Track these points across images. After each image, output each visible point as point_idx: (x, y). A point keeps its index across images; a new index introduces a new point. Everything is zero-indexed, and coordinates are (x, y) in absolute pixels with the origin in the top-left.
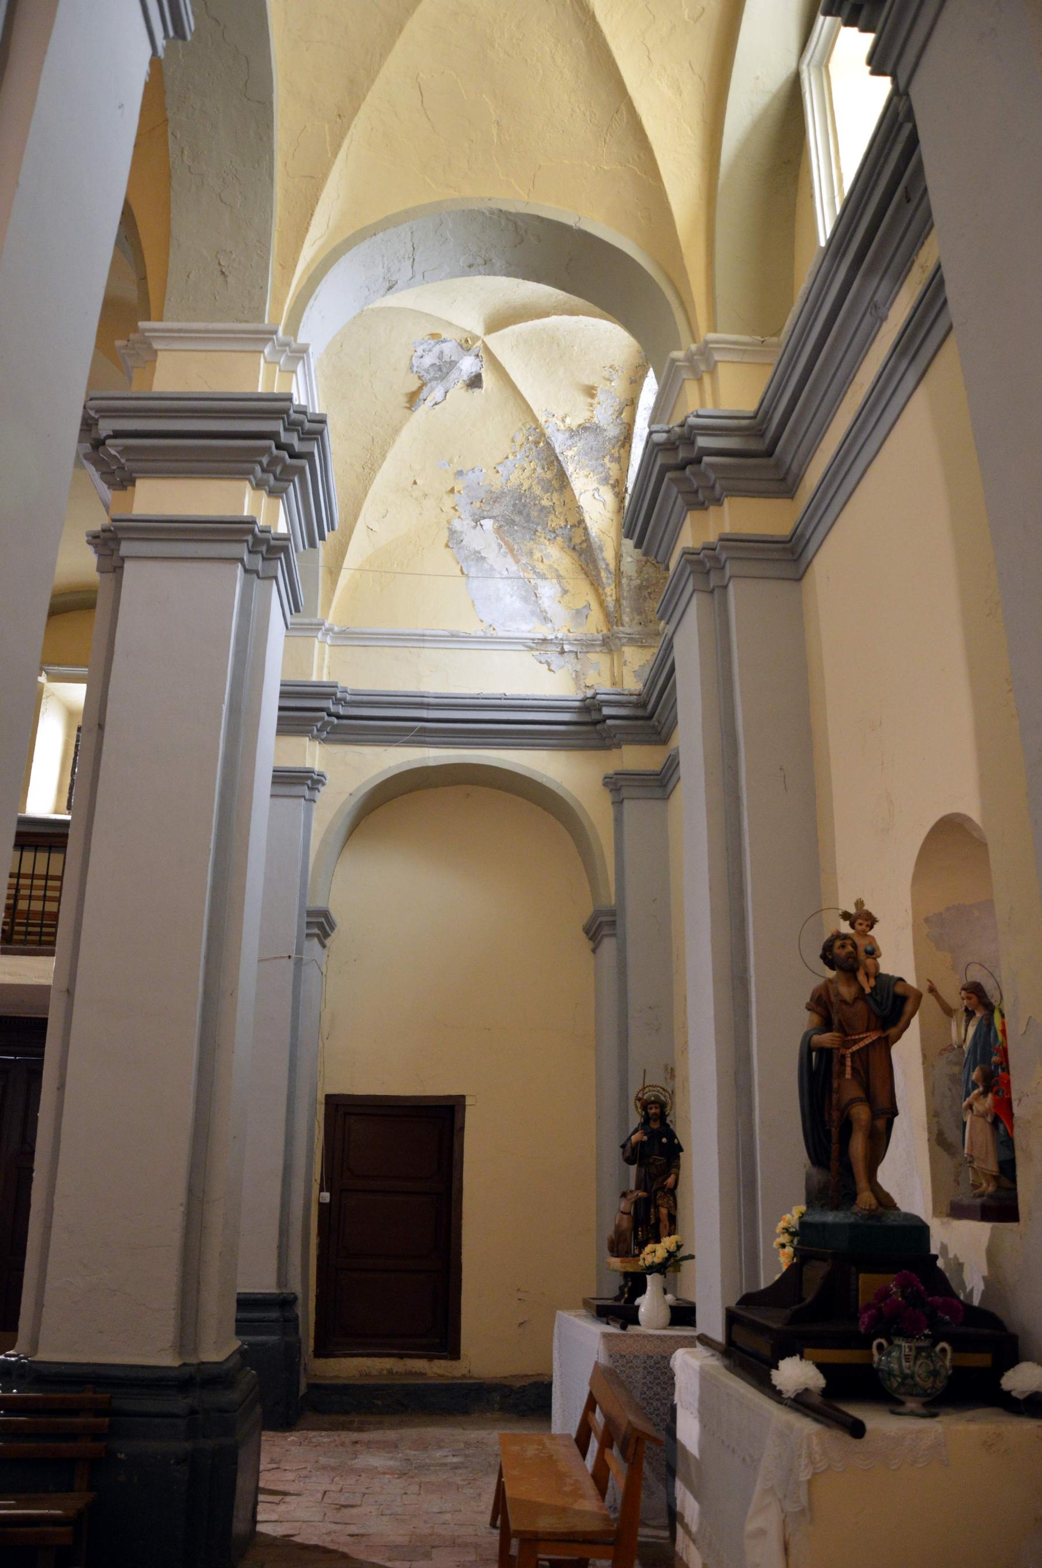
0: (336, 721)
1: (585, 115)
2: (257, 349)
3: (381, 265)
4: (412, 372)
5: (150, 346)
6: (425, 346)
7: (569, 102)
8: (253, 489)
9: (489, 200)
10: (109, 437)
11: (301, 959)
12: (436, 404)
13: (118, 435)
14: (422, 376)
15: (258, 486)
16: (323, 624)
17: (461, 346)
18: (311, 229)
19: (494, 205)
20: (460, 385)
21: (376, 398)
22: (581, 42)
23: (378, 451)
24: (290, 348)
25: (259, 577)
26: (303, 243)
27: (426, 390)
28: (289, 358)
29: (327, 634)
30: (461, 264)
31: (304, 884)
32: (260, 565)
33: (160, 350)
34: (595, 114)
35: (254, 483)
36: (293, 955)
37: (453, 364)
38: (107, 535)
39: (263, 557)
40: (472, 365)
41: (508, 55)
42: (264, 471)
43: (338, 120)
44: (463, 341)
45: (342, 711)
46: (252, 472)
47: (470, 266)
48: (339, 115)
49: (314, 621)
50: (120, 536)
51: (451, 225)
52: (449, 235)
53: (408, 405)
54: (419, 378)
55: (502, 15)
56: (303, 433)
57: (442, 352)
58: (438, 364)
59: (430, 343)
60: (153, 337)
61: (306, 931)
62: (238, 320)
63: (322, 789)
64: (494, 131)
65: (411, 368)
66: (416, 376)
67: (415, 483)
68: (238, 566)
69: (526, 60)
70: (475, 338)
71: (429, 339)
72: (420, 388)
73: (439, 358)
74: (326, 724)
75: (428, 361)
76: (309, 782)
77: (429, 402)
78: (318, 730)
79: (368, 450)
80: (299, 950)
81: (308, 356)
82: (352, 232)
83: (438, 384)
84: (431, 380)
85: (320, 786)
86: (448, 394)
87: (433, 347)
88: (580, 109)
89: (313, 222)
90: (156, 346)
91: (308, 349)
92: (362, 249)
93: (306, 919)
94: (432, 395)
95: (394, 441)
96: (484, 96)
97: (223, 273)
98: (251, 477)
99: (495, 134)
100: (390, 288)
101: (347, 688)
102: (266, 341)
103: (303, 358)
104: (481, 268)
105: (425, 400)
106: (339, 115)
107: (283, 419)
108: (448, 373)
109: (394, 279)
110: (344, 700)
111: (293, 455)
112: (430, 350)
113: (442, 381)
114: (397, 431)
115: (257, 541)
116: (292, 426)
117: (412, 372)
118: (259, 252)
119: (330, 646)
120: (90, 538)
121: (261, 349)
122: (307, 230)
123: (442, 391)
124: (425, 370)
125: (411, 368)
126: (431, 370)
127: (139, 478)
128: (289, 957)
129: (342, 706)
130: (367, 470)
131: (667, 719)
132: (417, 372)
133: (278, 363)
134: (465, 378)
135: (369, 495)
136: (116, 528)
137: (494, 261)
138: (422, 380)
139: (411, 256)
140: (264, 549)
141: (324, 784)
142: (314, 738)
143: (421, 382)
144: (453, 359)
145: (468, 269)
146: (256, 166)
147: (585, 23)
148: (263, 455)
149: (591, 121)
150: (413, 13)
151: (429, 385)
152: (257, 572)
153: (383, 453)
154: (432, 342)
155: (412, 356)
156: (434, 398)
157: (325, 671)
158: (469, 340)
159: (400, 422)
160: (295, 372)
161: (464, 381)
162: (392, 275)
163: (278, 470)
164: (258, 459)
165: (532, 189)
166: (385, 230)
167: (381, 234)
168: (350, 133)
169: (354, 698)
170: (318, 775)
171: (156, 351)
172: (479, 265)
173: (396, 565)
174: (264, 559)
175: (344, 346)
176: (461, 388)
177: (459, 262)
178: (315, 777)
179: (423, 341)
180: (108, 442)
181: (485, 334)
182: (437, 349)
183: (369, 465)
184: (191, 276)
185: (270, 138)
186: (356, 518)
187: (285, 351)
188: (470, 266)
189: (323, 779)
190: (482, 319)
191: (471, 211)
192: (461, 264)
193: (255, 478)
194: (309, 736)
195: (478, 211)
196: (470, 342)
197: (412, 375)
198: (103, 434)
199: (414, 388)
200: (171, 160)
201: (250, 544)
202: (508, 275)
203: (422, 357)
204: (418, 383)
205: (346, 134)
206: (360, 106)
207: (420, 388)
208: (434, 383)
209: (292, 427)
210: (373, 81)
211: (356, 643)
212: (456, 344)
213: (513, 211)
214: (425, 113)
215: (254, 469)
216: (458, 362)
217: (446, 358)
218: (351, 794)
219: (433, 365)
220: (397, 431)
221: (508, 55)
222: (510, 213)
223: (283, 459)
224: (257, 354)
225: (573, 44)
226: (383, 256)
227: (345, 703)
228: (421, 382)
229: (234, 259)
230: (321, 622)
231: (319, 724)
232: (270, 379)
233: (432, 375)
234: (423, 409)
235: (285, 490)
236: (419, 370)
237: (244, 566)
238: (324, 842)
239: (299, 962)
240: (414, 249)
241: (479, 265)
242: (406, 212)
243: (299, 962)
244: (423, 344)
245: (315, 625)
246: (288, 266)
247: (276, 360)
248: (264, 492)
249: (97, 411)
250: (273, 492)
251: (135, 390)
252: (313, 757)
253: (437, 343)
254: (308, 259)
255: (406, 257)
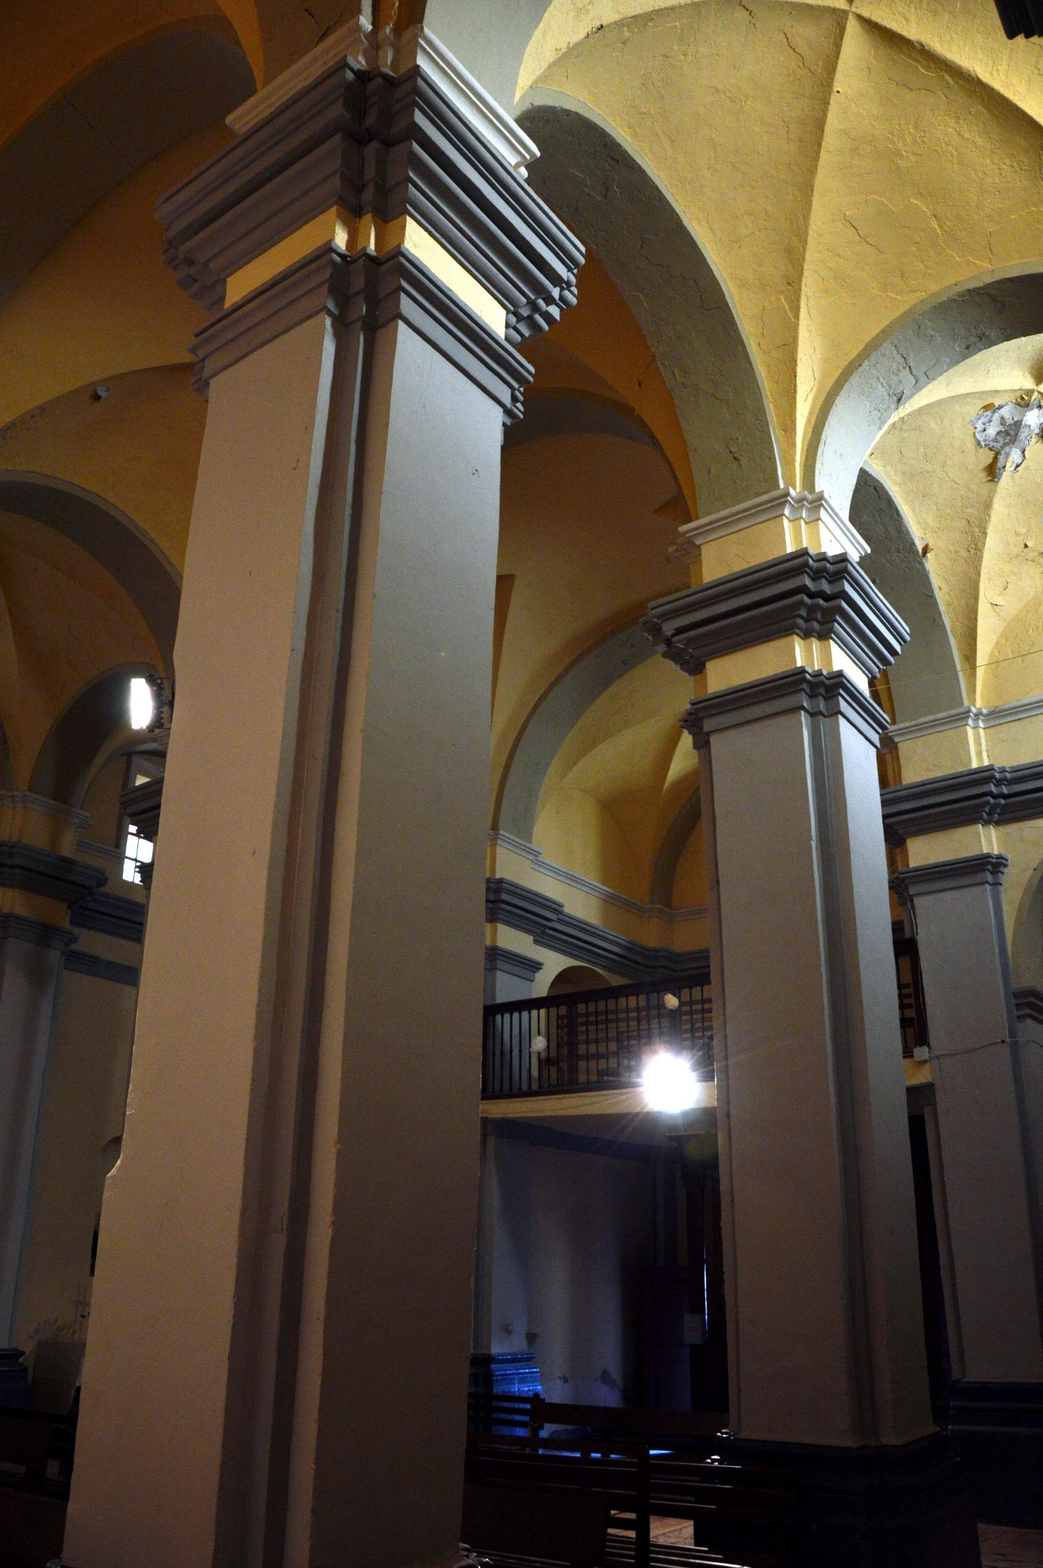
0: (1002, 801)
1: (1013, 167)
2: (778, 514)
3: (880, 386)
4: (981, 447)
5: (694, 543)
6: (983, 420)
7: (993, 163)
8: (803, 639)
9: (956, 285)
10: (674, 635)
11: (1016, 1042)
12: (1018, 466)
13: (680, 631)
14: (993, 447)
15: (806, 635)
16: (969, 711)
17: (1019, 405)
18: (799, 389)
19: (960, 289)
20: (1034, 439)
21: (957, 483)
22: (980, 107)
23: (978, 530)
24: (807, 501)
25: (825, 716)
26: (795, 403)
27: (1001, 458)
28: (809, 509)
29: (978, 719)
30: (958, 350)
31: (1005, 966)
32: (822, 705)
33: (702, 544)
34: (1021, 161)
35: (802, 634)
36: (1007, 1040)
37: (1018, 425)
38: (693, 717)
39: (824, 697)
40: (1038, 417)
41: (917, 155)
42: (806, 621)
43: (789, 287)
44: (1019, 400)
45: (1005, 790)
46: (796, 626)
47: (967, 348)
48: (789, 283)
49: (961, 710)
50: (701, 716)
51: (929, 324)
52: (932, 332)
53: (990, 478)
54: (990, 449)
55: (897, 127)
56: (830, 577)
57: (1002, 418)
58: (1003, 430)
59: (987, 415)
60: (693, 536)
61: (1016, 1013)
62: (758, 494)
63: (1006, 870)
64: (934, 224)
65: (979, 443)
66: (987, 448)
67: (1026, 546)
68: (801, 714)
69: (937, 151)
70: (1030, 392)
71: (984, 412)
72: (996, 459)
73: (1002, 424)
74: (993, 807)
75: (992, 431)
76: (990, 867)
77: (1010, 467)
78: (987, 814)
79: (966, 533)
80: (1012, 1032)
81: (826, 501)
82: (839, 372)
83: (1011, 448)
84: (1002, 448)
85: (1002, 869)
86: (1026, 453)
87: (991, 417)
88: (1005, 164)
89: (798, 382)
90: (698, 543)
91: (823, 496)
92: (855, 379)
93: (1014, 1002)
94: (1010, 460)
95: (989, 516)
96: (912, 200)
97: (735, 458)
98: (797, 631)
99: (936, 226)
100: (899, 400)
101: (1004, 767)
102: (783, 505)
103: (822, 505)
104: (979, 345)
105: (1004, 467)
106: (789, 283)
107: (806, 572)
108: (1017, 434)
109: (899, 391)
110: (1005, 779)
111: (827, 598)
112: (990, 421)
113: (1013, 443)
114: (988, 505)
115: (813, 686)
116: (817, 575)
117: (981, 447)
118: (760, 428)
119: (984, 729)
120: (682, 723)
121: (780, 513)
122: (795, 391)
123: (1019, 452)
124: (993, 441)
125: (979, 443)
126: (999, 438)
127: (708, 660)
128: (1003, 1042)
129: (1006, 785)
130: (972, 551)
131: (623, 940)
132: (985, 445)
133: (802, 518)
134: (1037, 431)
135: (982, 574)
136: (697, 710)
137: (987, 333)
138: (993, 451)
139: (905, 365)
140: (822, 691)
141: (1006, 866)
142: (986, 823)
143: (994, 452)
144: (1016, 419)
145: (966, 351)
146: (734, 359)
147: (975, 91)
148: (799, 609)
149: (1021, 169)
150: (816, 170)
151: (1003, 452)
152: (821, 713)
153: (982, 530)
154: (989, 413)
155: (974, 434)
156: (1014, 462)
157: (985, 755)
158: (1024, 396)
159: (989, 496)
160: (819, 519)
161: (1036, 434)
162: (895, 389)
163: (819, 616)
164: (796, 613)
165: (991, 257)
166: (868, 357)
167: (866, 362)
168: (803, 293)
169: (1015, 775)
170: (997, 858)
171: (699, 547)
172: (975, 343)
173: (1031, 631)
174: (825, 699)
175: (903, 452)
176: (1037, 442)
177: (955, 349)
178: (994, 861)
179: (978, 417)
180: (674, 639)
181: (1037, 385)
182: (996, 416)
183: (973, 546)
184: (712, 471)
185: (736, 331)
186: (976, 599)
187: (804, 505)
188: (967, 348)
189: (1003, 861)
190: (1027, 373)
191: (942, 304)
192: (958, 350)
193: (801, 630)
194: (980, 823)
195: (948, 300)
196: (1026, 398)
197: (981, 451)
198: (669, 633)
199: (990, 461)
200: (667, 384)
201: (808, 691)
202: (1008, 338)
203: (984, 430)
204: (992, 455)
205: (799, 296)
206: (802, 267)
207: (996, 459)
208: (1007, 449)
209: (818, 575)
210: (806, 241)
211: (1009, 719)
212: (1013, 406)
213: (981, 284)
214: (866, 241)
215: (796, 622)
216: (1022, 421)
217: (1009, 422)
218: (1035, 869)
219: (999, 433)
220: (988, 505)
221: (917, 155)
222: (979, 288)
223: (819, 606)
224: (780, 518)
225: (973, 113)
226: (878, 378)
227: (1007, 782)
228: (994, 452)
229: (742, 443)
230: (967, 709)
231: (987, 809)
232: (797, 533)
233: (1002, 442)
234: (1006, 478)
235: (832, 630)
236: (987, 443)
237: (806, 711)
238: (1018, 923)
239: (1015, 1046)
240: (905, 358)
241: (975, 343)
242: (883, 332)
243: (1015, 1046)
244: (980, 419)
245: (963, 714)
246: (789, 429)
247: (799, 516)
248: (814, 639)
249: (658, 618)
250: (822, 636)
251: (695, 587)
252: (990, 842)
253: (994, 412)
254: (806, 414)
255: (901, 368)
